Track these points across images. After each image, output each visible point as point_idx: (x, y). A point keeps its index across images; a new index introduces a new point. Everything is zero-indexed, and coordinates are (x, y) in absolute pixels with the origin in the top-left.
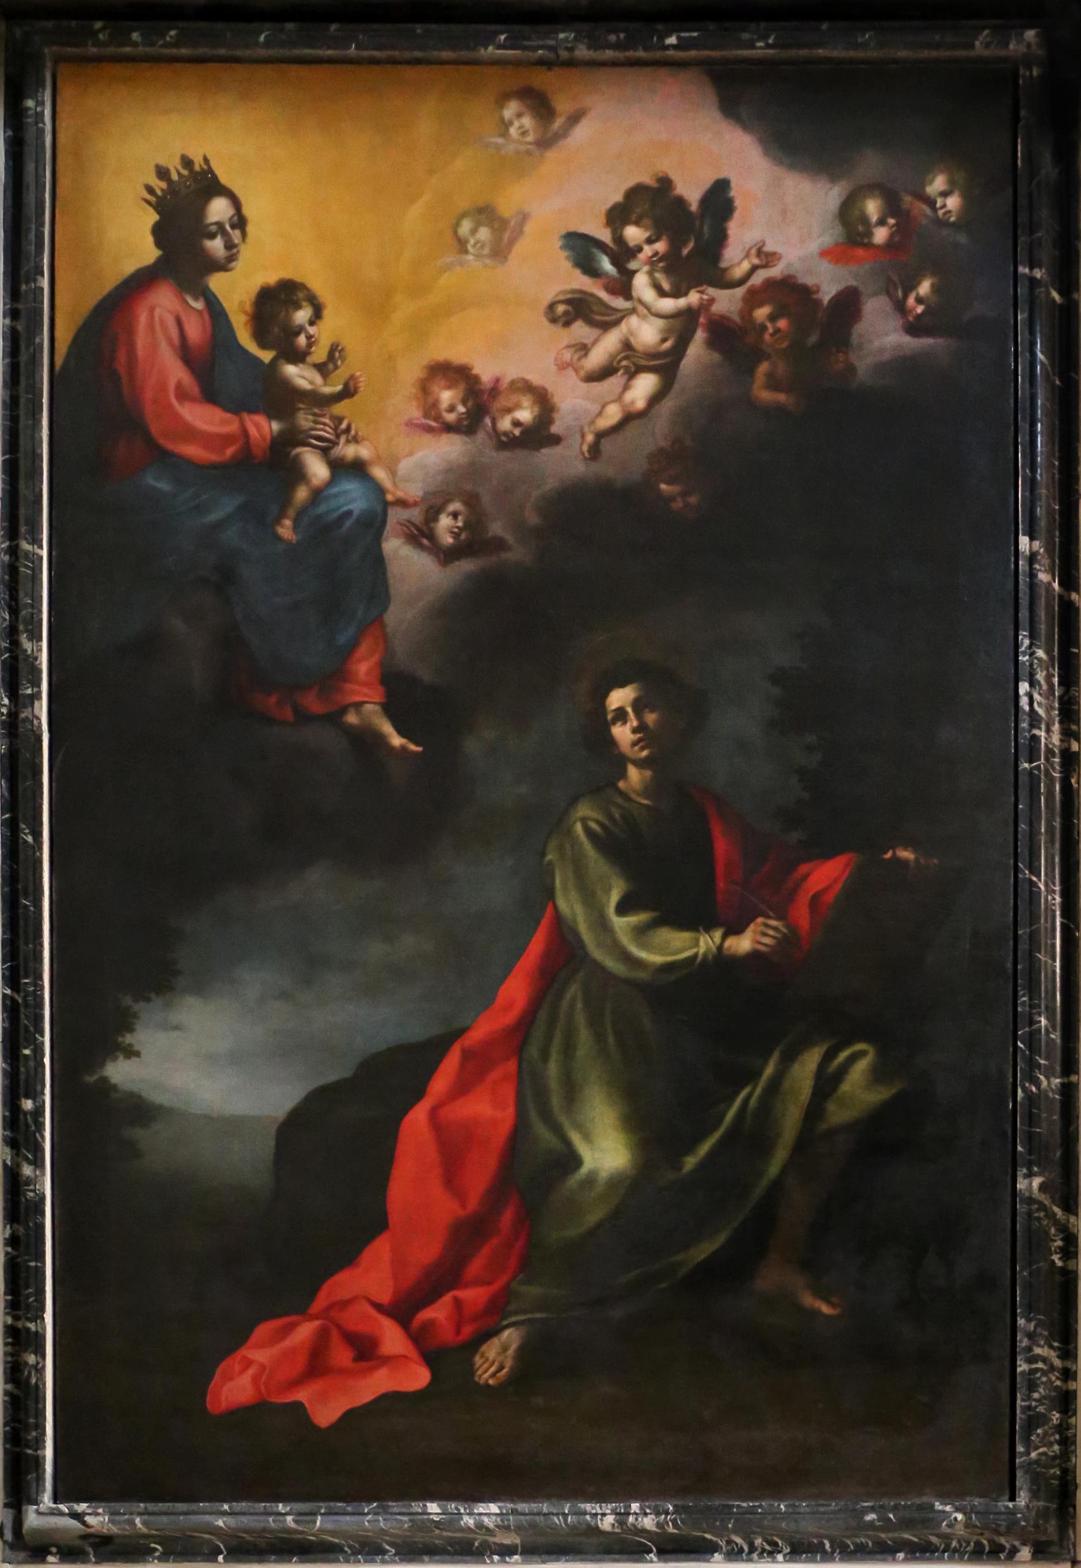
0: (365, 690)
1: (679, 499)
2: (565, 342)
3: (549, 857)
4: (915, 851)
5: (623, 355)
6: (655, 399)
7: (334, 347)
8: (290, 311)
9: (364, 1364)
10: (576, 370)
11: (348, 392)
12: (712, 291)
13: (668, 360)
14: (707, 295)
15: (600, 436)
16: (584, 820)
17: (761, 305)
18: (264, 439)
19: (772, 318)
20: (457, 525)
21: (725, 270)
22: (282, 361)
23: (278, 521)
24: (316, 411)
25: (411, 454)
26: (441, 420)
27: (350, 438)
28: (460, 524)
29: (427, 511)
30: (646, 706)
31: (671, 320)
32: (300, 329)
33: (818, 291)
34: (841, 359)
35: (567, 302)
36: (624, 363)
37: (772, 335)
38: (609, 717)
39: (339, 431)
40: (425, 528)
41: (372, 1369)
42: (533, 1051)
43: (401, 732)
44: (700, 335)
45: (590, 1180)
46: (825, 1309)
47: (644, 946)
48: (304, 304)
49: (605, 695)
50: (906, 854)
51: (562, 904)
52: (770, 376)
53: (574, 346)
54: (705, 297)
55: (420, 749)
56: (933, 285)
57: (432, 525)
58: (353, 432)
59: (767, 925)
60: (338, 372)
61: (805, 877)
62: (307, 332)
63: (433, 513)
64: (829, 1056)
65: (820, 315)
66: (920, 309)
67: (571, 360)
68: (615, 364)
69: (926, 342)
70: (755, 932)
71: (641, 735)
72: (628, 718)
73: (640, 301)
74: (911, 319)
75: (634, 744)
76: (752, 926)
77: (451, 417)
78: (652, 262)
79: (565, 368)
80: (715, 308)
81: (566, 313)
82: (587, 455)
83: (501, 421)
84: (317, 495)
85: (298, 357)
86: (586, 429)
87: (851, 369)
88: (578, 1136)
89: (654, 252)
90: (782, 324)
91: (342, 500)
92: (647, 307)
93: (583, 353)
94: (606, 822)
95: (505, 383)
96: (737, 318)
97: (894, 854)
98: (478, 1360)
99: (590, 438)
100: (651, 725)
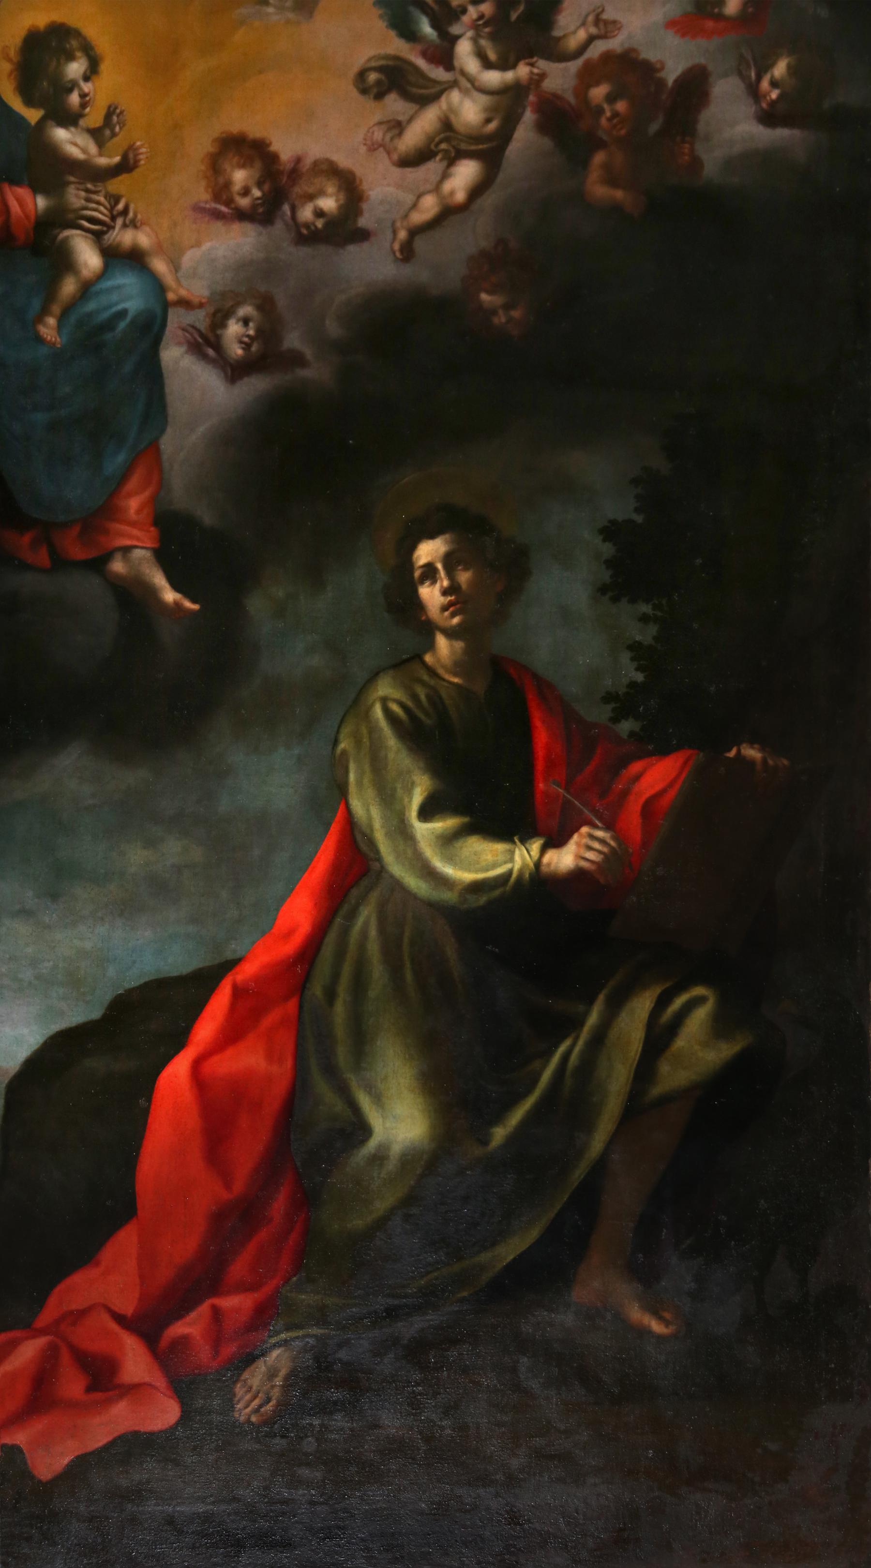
0: (135, 532)
1: (501, 312)
2: (377, 118)
3: (342, 746)
4: (762, 750)
5: (442, 136)
6: (476, 191)
7: (112, 109)
8: (62, 61)
9: (99, 1396)
10: (389, 153)
11: (126, 166)
12: (543, 64)
13: (494, 144)
14: (538, 68)
15: (415, 232)
16: (384, 700)
17: (597, 84)
18: (27, 217)
19: (611, 98)
20: (247, 333)
21: (559, 39)
22: (50, 123)
23: (40, 319)
24: (89, 186)
25: (198, 244)
26: (233, 206)
27: (127, 222)
28: (251, 332)
29: (214, 314)
30: (459, 563)
31: (496, 98)
32: (73, 86)
33: (662, 68)
34: (686, 151)
35: (379, 69)
36: (443, 146)
37: (609, 120)
38: (417, 574)
39: (115, 213)
40: (210, 336)
41: (107, 1403)
42: (317, 989)
43: (176, 586)
44: (529, 116)
45: (379, 1157)
46: (657, 1327)
47: (450, 859)
48: (78, 54)
49: (413, 547)
50: (752, 753)
51: (357, 805)
52: (606, 167)
53: (388, 122)
54: (536, 71)
55: (195, 607)
56: (789, 67)
57: (219, 332)
58: (131, 215)
59: (592, 837)
60: (115, 140)
61: (638, 778)
62: (80, 89)
63: (220, 319)
64: (662, 1002)
65: (664, 97)
66: (774, 95)
67: (383, 140)
68: (432, 147)
69: (781, 134)
70: (578, 844)
71: (453, 598)
72: (438, 576)
73: (463, 73)
74: (764, 105)
75: (444, 608)
76: (576, 837)
77: (244, 202)
78: (475, 26)
79: (375, 150)
80: (548, 85)
81: (378, 83)
82: (398, 254)
83: (301, 210)
84: (87, 289)
85: (69, 119)
86: (398, 224)
87: (696, 163)
88: (367, 1099)
89: (480, 14)
90: (621, 106)
91: (115, 297)
92: (471, 80)
93: (396, 131)
94: (410, 703)
95: (308, 162)
96: (572, 100)
97: (739, 751)
98: (239, 1390)
99: (402, 235)
100: (464, 586)
